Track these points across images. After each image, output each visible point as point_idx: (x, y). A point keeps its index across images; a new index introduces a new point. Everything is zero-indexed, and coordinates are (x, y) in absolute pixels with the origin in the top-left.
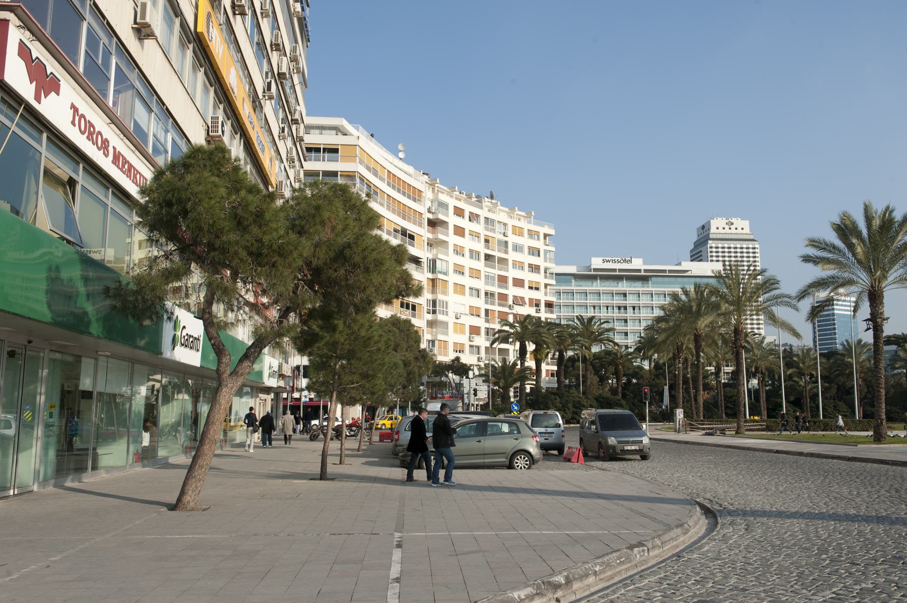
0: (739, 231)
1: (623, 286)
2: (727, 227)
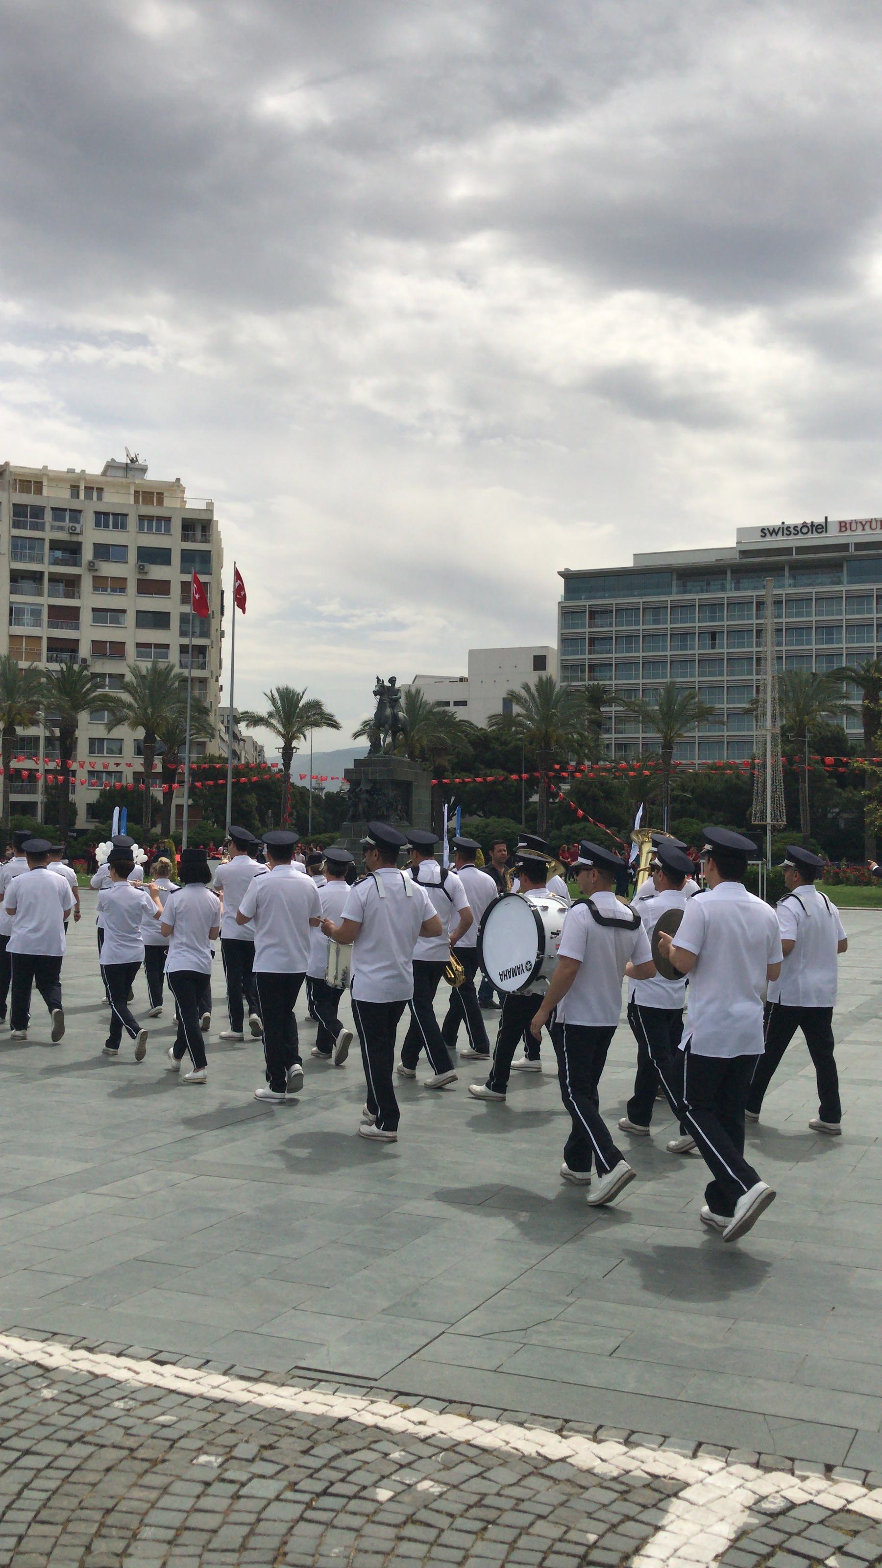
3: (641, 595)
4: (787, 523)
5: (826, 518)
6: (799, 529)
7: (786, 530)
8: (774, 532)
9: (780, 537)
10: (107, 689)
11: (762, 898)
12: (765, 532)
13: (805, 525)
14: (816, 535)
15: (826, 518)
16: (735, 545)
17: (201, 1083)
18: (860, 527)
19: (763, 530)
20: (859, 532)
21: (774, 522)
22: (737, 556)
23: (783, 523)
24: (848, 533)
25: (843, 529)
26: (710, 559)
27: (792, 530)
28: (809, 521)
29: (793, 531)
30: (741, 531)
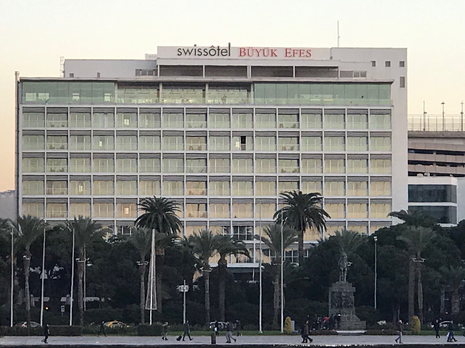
1: (213, 98)
4: (199, 45)
5: (229, 44)
6: (208, 51)
7: (198, 51)
8: (188, 52)
10: (253, 281)
12: (180, 51)
13: (212, 48)
14: (221, 57)
15: (229, 44)
17: (195, 55)
18: (255, 53)
20: (255, 56)
21: (188, 44)
22: (175, 54)
23: (195, 45)
24: (246, 57)
25: (243, 54)
27: (202, 51)
28: (216, 46)
29: (203, 53)
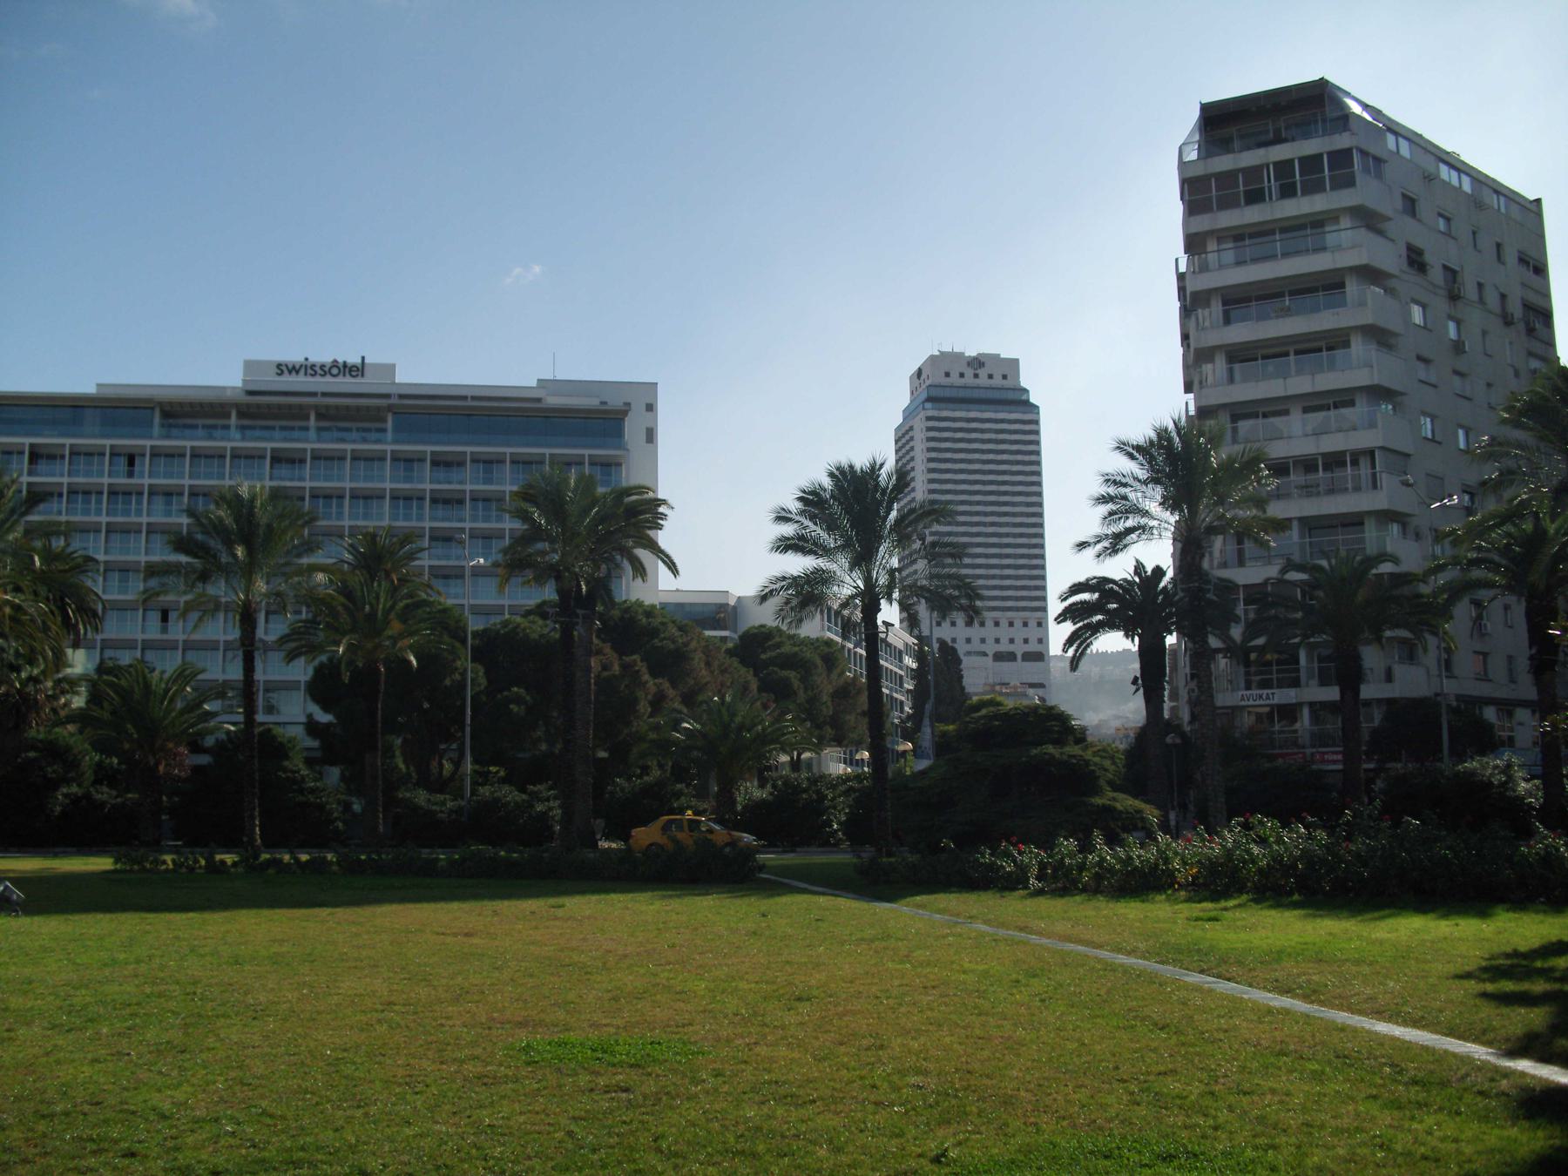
0: (997, 381)
2: (969, 373)
3: (27, 435)
7: (310, 369)
8: (294, 369)
9: (301, 378)
11: (897, 451)
12: (282, 368)
13: (335, 364)
16: (240, 384)
19: (279, 366)
21: (295, 356)
26: (592, 402)
30: (249, 365)
